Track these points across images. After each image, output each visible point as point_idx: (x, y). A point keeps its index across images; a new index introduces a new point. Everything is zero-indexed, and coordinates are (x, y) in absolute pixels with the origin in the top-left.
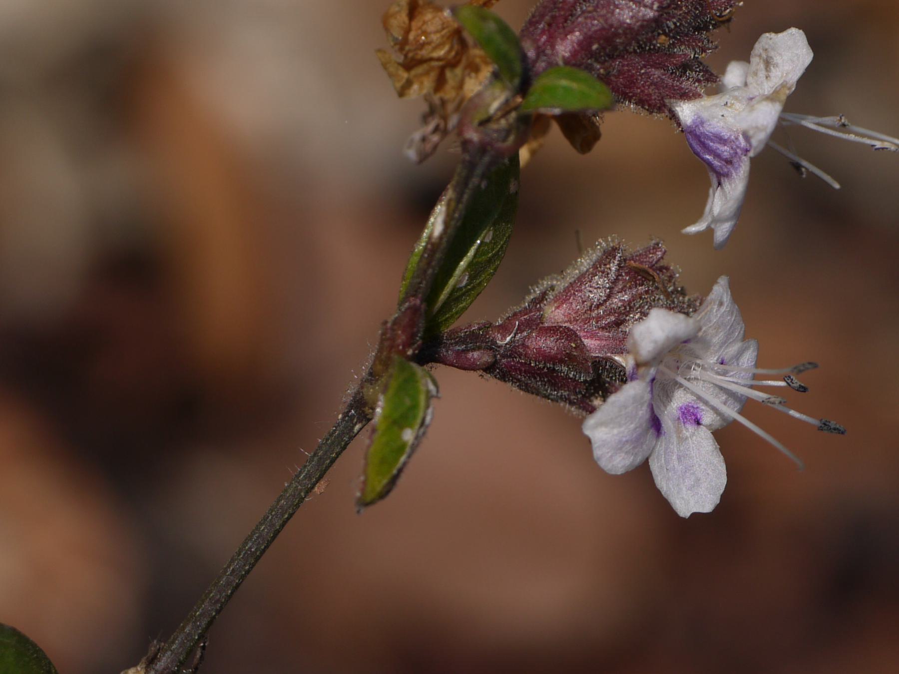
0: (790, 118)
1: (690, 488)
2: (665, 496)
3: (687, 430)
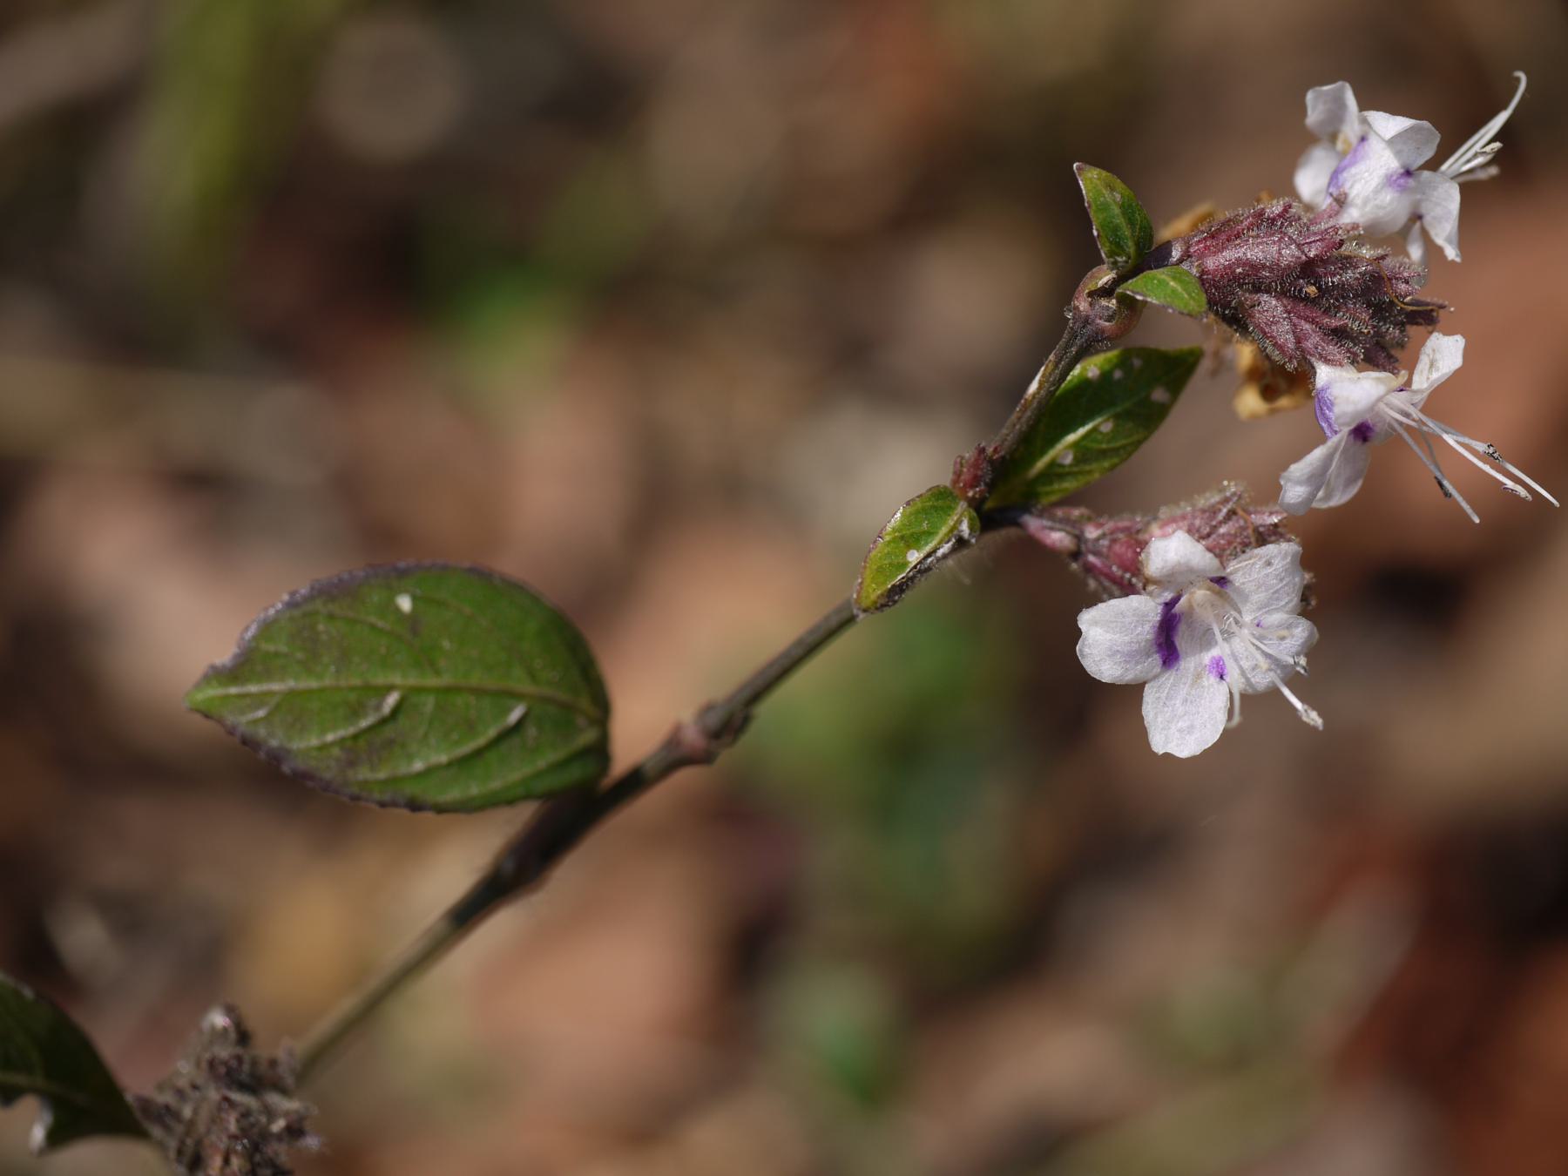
0: (1431, 425)
2: (1147, 725)
3: (1208, 680)
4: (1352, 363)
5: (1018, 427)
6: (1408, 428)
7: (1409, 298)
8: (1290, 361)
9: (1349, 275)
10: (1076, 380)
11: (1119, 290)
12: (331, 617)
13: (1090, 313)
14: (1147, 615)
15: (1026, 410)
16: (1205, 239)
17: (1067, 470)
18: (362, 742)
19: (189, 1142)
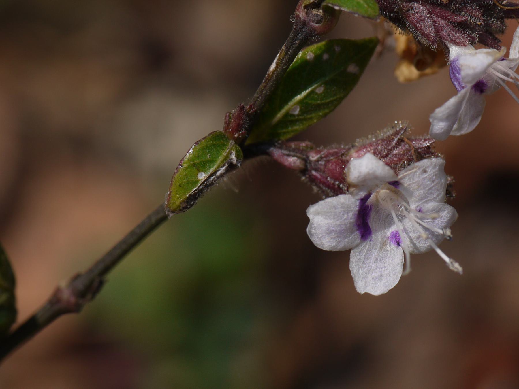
2: (353, 276)
3: (390, 246)
4: (472, 44)
8: (433, 44)
14: (350, 207)
15: (269, 81)
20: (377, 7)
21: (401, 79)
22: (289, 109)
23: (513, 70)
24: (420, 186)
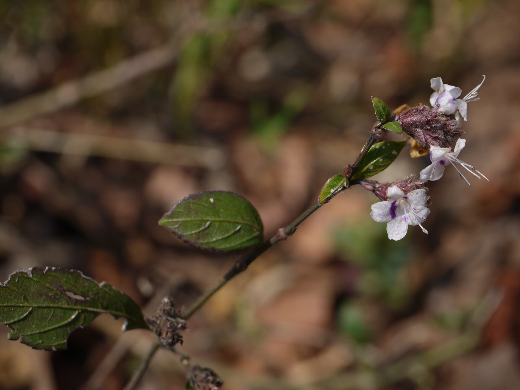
0: (459, 162)
1: (396, 234)
4: (439, 146)
5: (359, 160)
6: (453, 162)
7: (453, 130)
8: (424, 145)
9: (438, 125)
10: (373, 149)
11: (381, 127)
12: (194, 203)
13: (375, 132)
14: (388, 206)
15: (361, 155)
16: (404, 115)
17: (371, 170)
18: (201, 234)
19: (159, 329)
20: (401, 129)
21: (412, 156)
22: (369, 167)
23: (455, 157)
24: (415, 199)
